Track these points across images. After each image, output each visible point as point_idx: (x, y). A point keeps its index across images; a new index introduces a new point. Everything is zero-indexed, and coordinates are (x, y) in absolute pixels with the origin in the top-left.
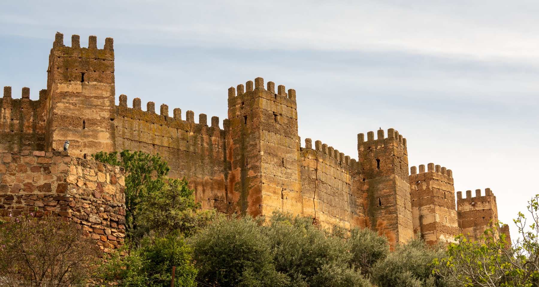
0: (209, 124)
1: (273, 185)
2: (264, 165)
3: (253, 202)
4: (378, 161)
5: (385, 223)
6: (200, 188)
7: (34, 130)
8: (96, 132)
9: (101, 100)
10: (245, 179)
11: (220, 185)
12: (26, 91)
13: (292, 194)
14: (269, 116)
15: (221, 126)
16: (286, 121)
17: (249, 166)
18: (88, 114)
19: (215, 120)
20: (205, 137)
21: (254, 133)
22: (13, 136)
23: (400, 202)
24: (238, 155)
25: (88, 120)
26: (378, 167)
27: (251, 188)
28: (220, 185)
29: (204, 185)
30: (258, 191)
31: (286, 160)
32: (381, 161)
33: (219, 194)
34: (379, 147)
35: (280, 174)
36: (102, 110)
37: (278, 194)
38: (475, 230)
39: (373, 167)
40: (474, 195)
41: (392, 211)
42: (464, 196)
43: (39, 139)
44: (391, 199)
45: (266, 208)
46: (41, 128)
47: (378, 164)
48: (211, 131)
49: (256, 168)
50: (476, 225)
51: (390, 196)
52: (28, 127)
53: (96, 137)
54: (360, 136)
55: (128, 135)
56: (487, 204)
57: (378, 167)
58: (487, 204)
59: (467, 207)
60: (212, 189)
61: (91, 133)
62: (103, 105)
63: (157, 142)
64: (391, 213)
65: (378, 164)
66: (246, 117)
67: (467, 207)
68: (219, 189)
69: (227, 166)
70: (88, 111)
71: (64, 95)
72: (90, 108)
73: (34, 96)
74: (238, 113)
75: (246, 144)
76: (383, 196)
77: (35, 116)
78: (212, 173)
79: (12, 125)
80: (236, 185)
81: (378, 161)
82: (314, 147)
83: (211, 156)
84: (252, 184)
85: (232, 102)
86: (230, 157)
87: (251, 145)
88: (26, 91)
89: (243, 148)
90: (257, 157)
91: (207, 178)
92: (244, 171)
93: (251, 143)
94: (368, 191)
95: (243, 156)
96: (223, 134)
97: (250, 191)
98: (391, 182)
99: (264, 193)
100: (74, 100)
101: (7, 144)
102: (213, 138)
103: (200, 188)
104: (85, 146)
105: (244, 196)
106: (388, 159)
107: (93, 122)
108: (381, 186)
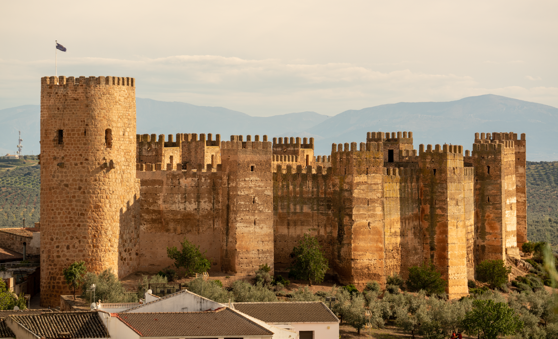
3: (440, 232)
4: (489, 167)
5: (492, 215)
7: (325, 195)
8: (374, 207)
9: (377, 186)
17: (437, 206)
18: (371, 196)
21: (443, 184)
22: (313, 199)
24: (428, 195)
25: (371, 199)
26: (488, 172)
27: (438, 222)
28: (416, 217)
30: (446, 225)
32: (491, 168)
33: (416, 224)
34: (490, 157)
35: (456, 211)
36: (378, 192)
39: (484, 172)
43: (328, 201)
44: (498, 198)
46: (329, 194)
47: (489, 170)
49: (445, 210)
51: (497, 195)
52: (322, 193)
53: (374, 210)
56: (522, 147)
57: (488, 172)
58: (522, 147)
60: (413, 221)
61: (372, 208)
62: (378, 189)
64: (497, 209)
65: (489, 170)
66: (435, 170)
70: (370, 194)
71: (358, 184)
72: (371, 192)
74: (428, 165)
75: (435, 190)
76: (491, 196)
78: (413, 210)
79: (313, 192)
80: (425, 216)
81: (489, 167)
83: (412, 199)
84: (440, 219)
86: (421, 196)
87: (440, 192)
89: (432, 192)
90: (445, 202)
92: (432, 208)
93: (439, 190)
95: (432, 197)
97: (438, 224)
98: (498, 186)
100: (363, 187)
101: (310, 205)
102: (413, 184)
103: (407, 222)
104: (369, 217)
105: (432, 225)
106: (497, 167)
108: (490, 187)
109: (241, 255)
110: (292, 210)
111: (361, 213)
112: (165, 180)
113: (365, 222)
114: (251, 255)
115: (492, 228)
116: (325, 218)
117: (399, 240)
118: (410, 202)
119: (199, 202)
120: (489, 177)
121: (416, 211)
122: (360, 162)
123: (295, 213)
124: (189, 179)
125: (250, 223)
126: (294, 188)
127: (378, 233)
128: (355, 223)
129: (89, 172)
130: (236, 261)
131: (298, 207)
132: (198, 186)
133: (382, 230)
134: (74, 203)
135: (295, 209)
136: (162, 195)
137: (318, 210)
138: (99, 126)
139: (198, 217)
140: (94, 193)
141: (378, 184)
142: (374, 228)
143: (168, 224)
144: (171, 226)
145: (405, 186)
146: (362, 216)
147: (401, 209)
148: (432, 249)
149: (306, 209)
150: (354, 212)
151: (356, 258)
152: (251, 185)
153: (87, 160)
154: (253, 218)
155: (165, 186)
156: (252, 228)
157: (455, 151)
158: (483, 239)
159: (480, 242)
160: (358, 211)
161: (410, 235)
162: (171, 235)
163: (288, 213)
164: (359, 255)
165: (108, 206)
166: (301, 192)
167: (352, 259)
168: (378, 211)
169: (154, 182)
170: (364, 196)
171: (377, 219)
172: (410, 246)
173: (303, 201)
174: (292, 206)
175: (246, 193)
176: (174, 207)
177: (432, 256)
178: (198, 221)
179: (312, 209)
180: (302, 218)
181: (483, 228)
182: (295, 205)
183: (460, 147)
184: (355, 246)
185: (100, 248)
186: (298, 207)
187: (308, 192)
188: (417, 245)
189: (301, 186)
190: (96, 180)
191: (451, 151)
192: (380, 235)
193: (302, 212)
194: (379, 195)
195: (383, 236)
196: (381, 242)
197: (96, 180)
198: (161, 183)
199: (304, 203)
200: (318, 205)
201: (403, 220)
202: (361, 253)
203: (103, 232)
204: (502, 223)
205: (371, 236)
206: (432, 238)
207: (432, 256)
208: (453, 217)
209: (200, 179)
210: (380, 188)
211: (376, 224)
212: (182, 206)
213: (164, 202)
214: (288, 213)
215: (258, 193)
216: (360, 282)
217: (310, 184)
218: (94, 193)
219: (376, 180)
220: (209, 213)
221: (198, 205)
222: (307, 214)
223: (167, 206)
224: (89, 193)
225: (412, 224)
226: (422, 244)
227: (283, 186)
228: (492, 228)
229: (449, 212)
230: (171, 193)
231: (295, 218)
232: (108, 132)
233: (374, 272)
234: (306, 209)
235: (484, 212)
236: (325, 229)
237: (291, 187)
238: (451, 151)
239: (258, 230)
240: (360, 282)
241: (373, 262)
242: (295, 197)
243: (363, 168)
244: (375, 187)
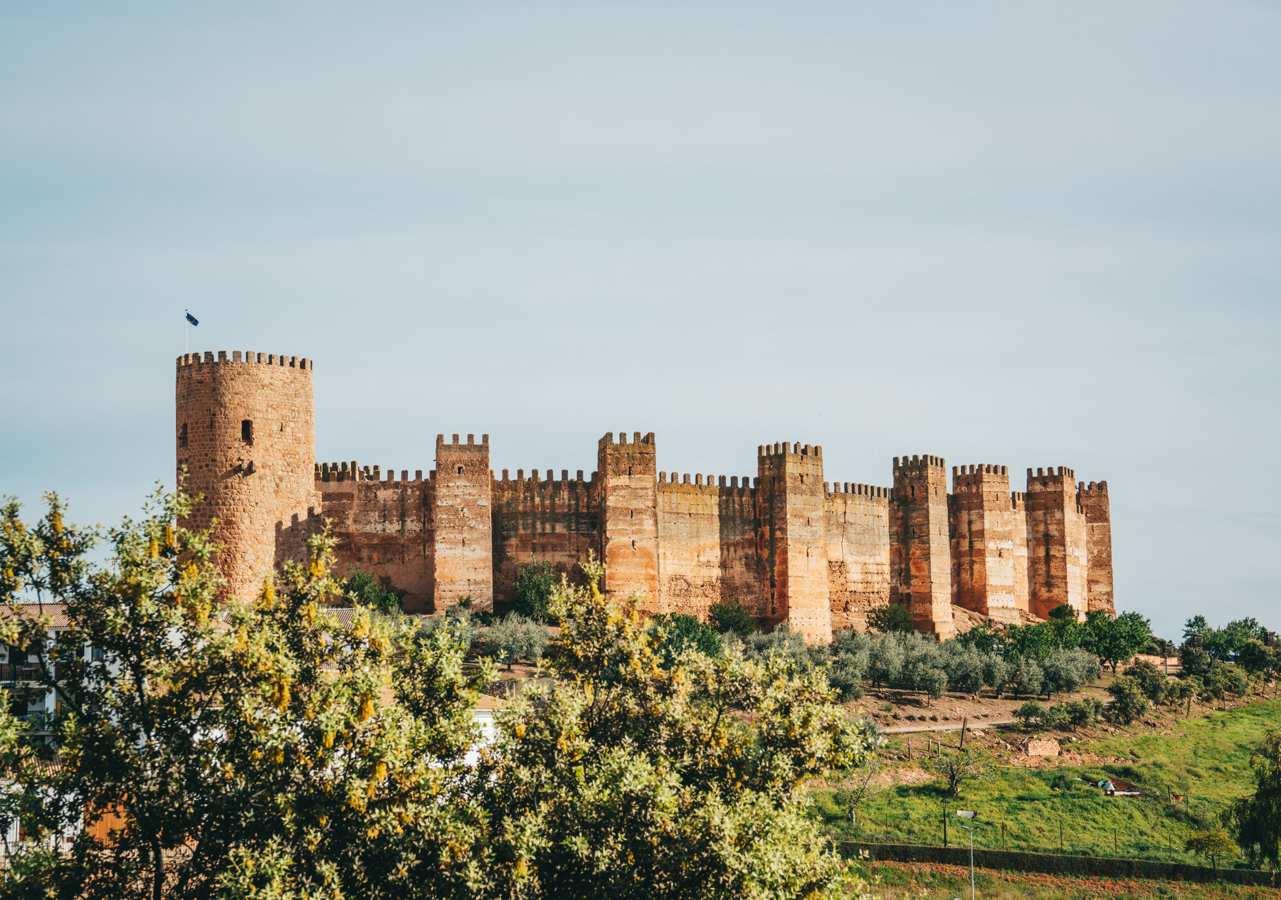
0: (740, 485)
1: (799, 546)
2: (789, 528)
6: (732, 549)
8: (641, 520)
10: (773, 540)
11: (750, 543)
12: (580, 473)
13: (818, 551)
14: (795, 479)
15: (751, 485)
16: (812, 480)
18: (635, 504)
19: (746, 480)
20: (736, 499)
23: (933, 529)
28: (750, 543)
29: (736, 545)
30: (785, 552)
38: (1045, 514)
40: (1046, 473)
41: (925, 541)
42: (1035, 474)
46: (594, 507)
48: (741, 492)
49: (784, 531)
50: (1046, 508)
54: (896, 460)
55: (667, 509)
59: (1038, 488)
60: (743, 548)
63: (693, 511)
67: (1038, 488)
68: (749, 547)
69: (757, 524)
71: (615, 488)
73: (587, 478)
77: (588, 496)
78: (743, 533)
79: (569, 505)
82: (843, 490)
83: (742, 517)
85: (762, 460)
88: (580, 473)
89: (772, 509)
90: (784, 520)
91: (738, 538)
92: (772, 531)
94: (902, 518)
96: (753, 492)
99: (790, 554)
100: (623, 492)
103: (732, 549)
105: (772, 554)
107: (640, 512)
108: (914, 514)
109: (442, 587)
110: (539, 530)
112: (356, 493)
113: (626, 540)
114: (457, 587)
115: (919, 569)
116: (588, 540)
117: (716, 572)
118: (738, 521)
119: (404, 521)
120: (914, 500)
121: (750, 535)
123: (543, 534)
124: (390, 492)
125: (456, 543)
126: (542, 501)
127: (648, 555)
129: (216, 477)
130: (436, 595)
131: (548, 526)
132: (402, 499)
133: (653, 551)
134: (199, 518)
135: (544, 529)
136: (351, 514)
137: (577, 529)
138: (231, 416)
139: (402, 541)
140: (224, 504)
143: (360, 550)
144: (365, 553)
145: (727, 501)
146: (622, 532)
147: (721, 532)
148: (773, 585)
149: (560, 529)
150: (609, 526)
152: (457, 492)
153: (214, 460)
154: (460, 537)
155: (356, 501)
156: (459, 551)
158: (908, 585)
159: (903, 589)
161: (738, 568)
162: (365, 565)
163: (534, 535)
165: (247, 521)
166: (553, 506)
168: (648, 524)
169: (340, 496)
170: (625, 505)
172: (738, 582)
173: (555, 518)
174: (539, 525)
175: (450, 503)
176: (369, 529)
177: (773, 595)
178: (403, 546)
179: (569, 528)
180: (555, 541)
181: (908, 570)
182: (543, 524)
185: (235, 576)
186: (548, 526)
187: (562, 506)
188: (751, 581)
189: (552, 498)
190: (226, 487)
193: (553, 533)
195: (655, 559)
196: (652, 567)
197: (226, 487)
198: (350, 496)
199: (559, 521)
200: (578, 523)
201: (725, 545)
202: (620, 582)
203: (238, 556)
205: (636, 560)
206: (772, 571)
207: (773, 595)
208: (798, 541)
209: (405, 490)
211: (646, 543)
212: (379, 527)
213: (355, 521)
214: (534, 535)
215: (467, 504)
217: (565, 494)
218: (224, 504)
220: (418, 536)
221: (403, 525)
222: (561, 536)
223: (359, 527)
224: (218, 504)
225: (740, 553)
226: (760, 579)
227: (525, 498)
228: (919, 569)
229: (789, 533)
230: (365, 509)
231: (544, 540)
232: (247, 427)
234: (560, 529)
235: (908, 549)
237: (537, 500)
239: (467, 552)
242: (544, 513)
243: (624, 466)
244: (641, 493)
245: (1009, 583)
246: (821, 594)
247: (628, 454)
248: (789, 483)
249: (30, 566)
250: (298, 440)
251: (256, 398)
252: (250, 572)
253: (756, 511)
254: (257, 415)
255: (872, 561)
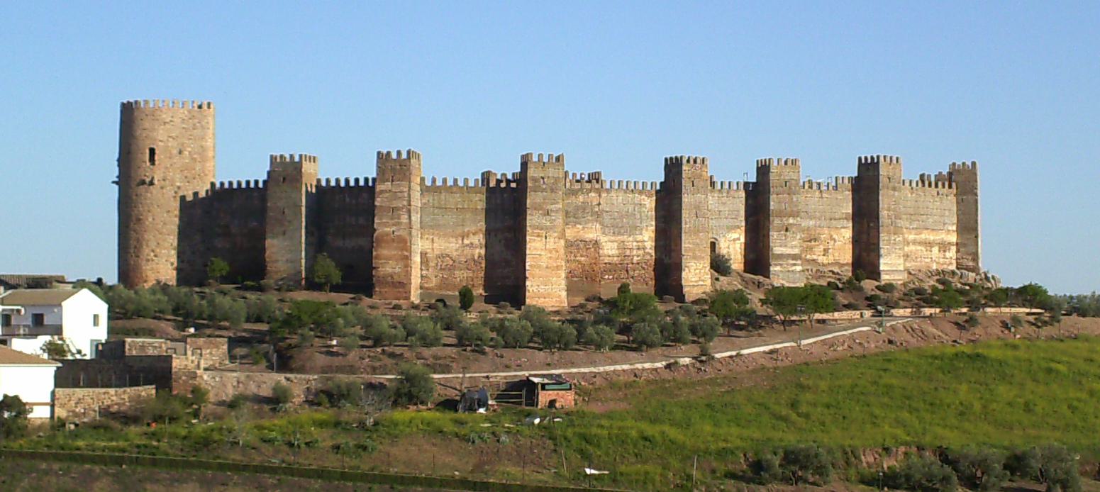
13: (556, 235)
31: (551, 210)
37: (542, 236)
45: (530, 249)
53: (399, 218)
55: (436, 205)
71: (382, 192)
100: (387, 195)
107: (398, 209)
111: (384, 221)
122: (384, 170)
128: (377, 232)
141: (404, 192)
142: (399, 236)
146: (386, 225)
151: (377, 266)
157: (310, 161)
160: (381, 219)
164: (381, 264)
165: (150, 219)
167: (375, 268)
171: (402, 227)
183: (314, 158)
184: (377, 255)
191: (306, 160)
192: (406, 243)
194: (405, 203)
195: (409, 244)
202: (383, 261)
204: (977, 237)
210: (406, 195)
216: (382, 290)
219: (401, 188)
232: (152, 151)
233: (399, 280)
236: (463, 240)
237: (348, 200)
238: (306, 160)
240: (382, 290)
241: (397, 270)
245: (796, 251)
246: (558, 268)
247: (394, 167)
248: (530, 184)
249: (899, 225)
250: (194, 160)
251: (160, 136)
252: (152, 254)
253: (506, 206)
254: (160, 143)
255: (631, 239)
